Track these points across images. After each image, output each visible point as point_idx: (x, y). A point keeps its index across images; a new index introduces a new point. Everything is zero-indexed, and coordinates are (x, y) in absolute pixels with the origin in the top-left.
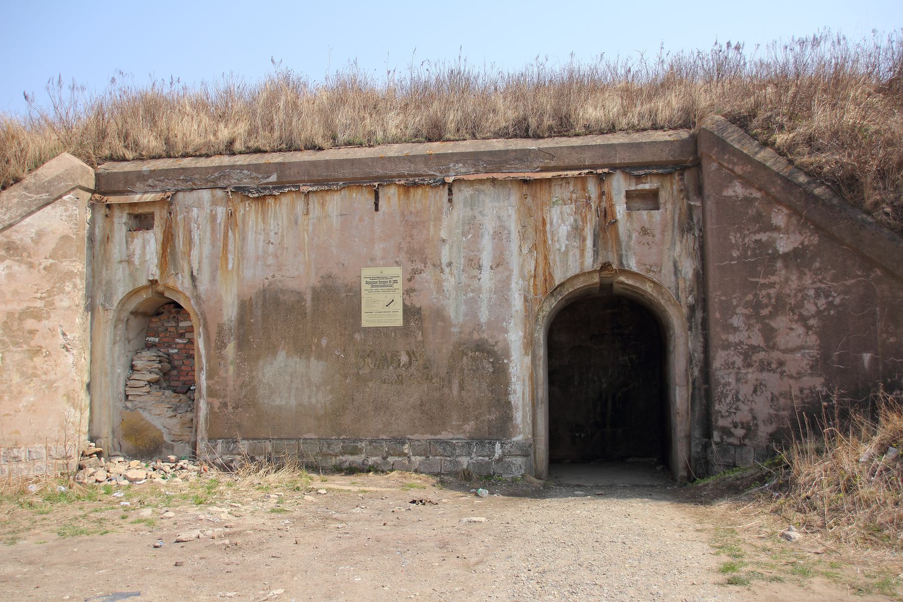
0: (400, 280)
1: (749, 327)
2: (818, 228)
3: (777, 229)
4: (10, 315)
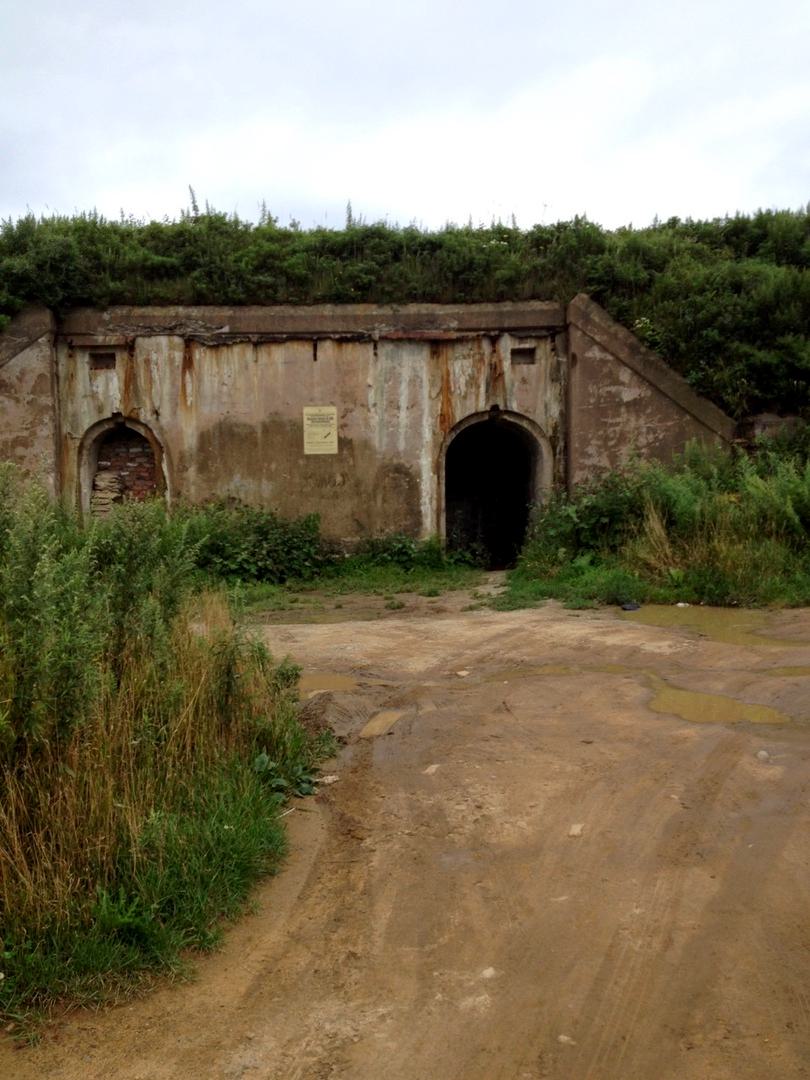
0: (335, 417)
1: (600, 454)
2: (651, 384)
3: (623, 384)
4: (5, 443)
